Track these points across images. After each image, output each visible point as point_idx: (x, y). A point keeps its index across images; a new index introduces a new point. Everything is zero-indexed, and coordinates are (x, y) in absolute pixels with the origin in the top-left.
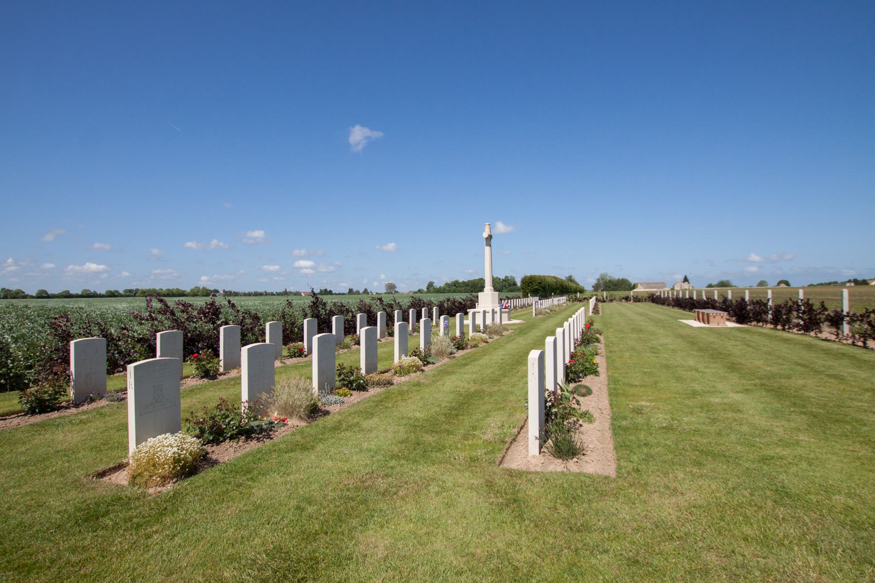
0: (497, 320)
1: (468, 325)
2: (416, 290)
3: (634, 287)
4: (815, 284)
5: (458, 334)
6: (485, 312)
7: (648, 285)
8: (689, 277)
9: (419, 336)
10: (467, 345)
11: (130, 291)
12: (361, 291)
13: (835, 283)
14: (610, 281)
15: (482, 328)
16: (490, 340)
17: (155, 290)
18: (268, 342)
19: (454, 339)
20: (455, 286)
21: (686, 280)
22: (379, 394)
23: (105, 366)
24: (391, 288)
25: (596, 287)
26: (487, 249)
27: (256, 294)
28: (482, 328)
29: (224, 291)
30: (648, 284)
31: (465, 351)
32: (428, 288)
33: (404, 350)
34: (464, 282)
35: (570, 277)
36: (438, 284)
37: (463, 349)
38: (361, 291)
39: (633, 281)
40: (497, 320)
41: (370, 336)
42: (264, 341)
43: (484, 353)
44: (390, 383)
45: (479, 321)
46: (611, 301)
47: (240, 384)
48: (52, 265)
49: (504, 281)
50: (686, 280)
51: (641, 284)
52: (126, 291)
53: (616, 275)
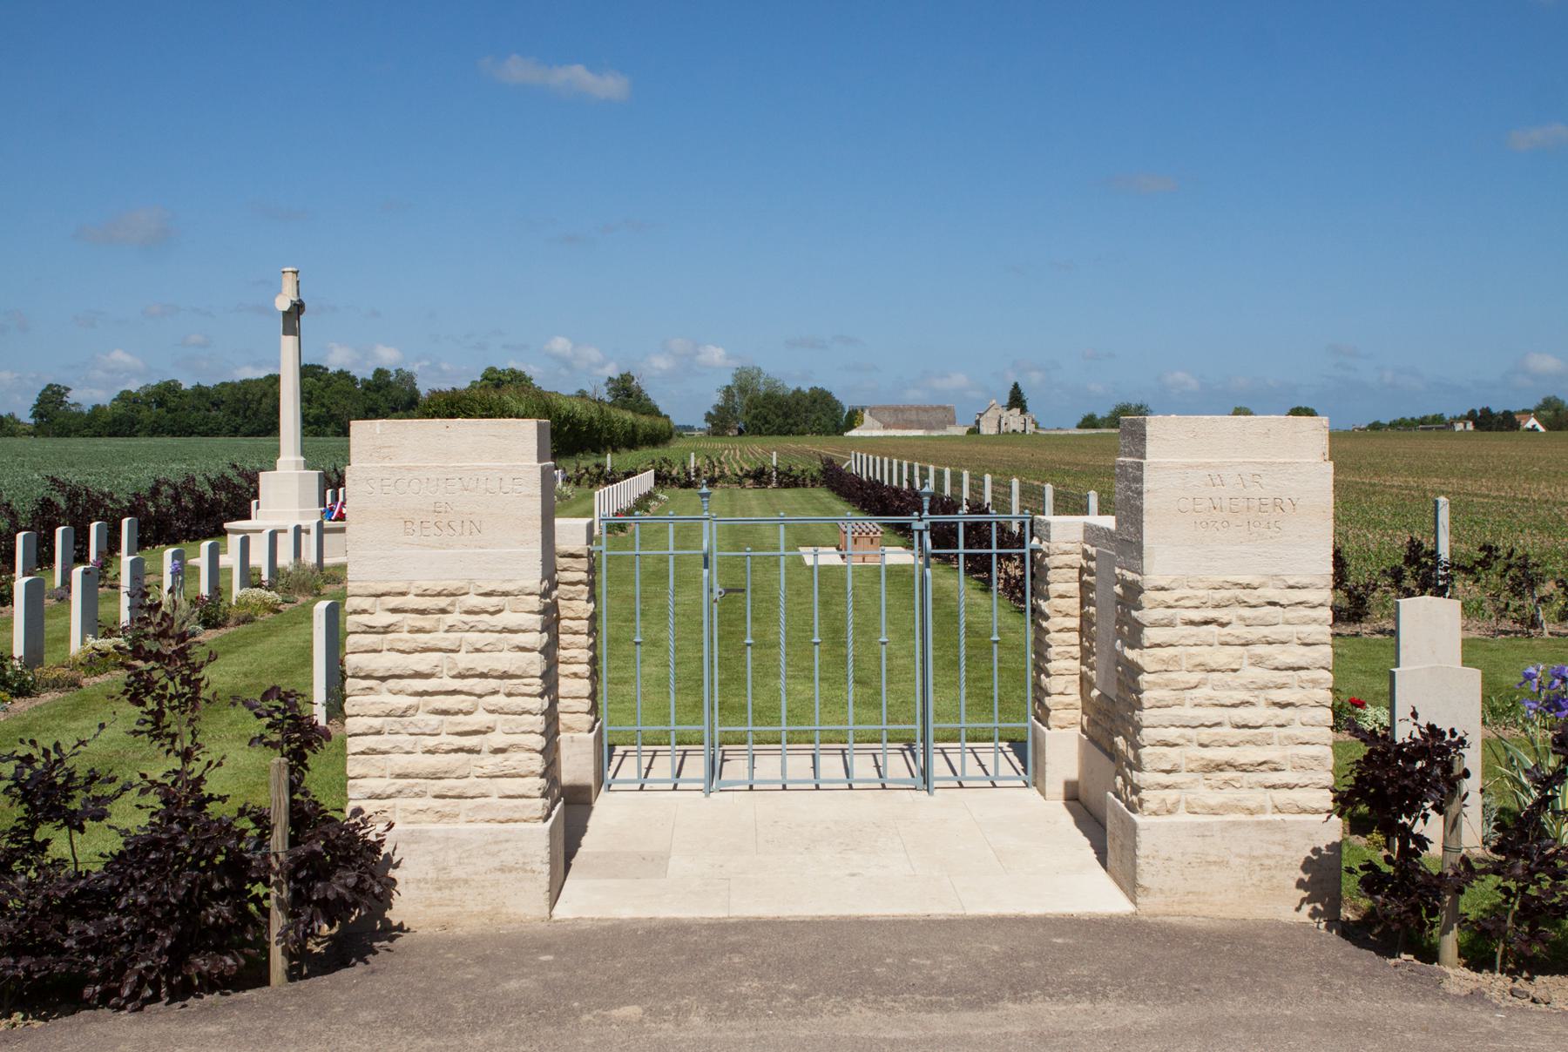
0: (309, 557)
1: (229, 570)
3: (853, 419)
4: (1386, 420)
5: (204, 590)
6: (273, 536)
7: (897, 415)
8: (1027, 395)
10: (227, 618)
13: (1438, 419)
14: (769, 397)
15: (265, 576)
16: (285, 607)
19: (196, 601)
20: (164, 412)
21: (1016, 400)
22: (55, 703)
25: (720, 422)
28: (265, 576)
30: (897, 410)
31: (223, 631)
33: (92, 624)
34: (200, 391)
35: (626, 379)
37: (217, 626)
39: (848, 402)
40: (309, 557)
41: (35, 593)
43: (269, 631)
44: (75, 684)
45: (259, 559)
46: (712, 482)
49: (368, 386)
50: (1016, 400)
51: (874, 411)
53: (792, 371)
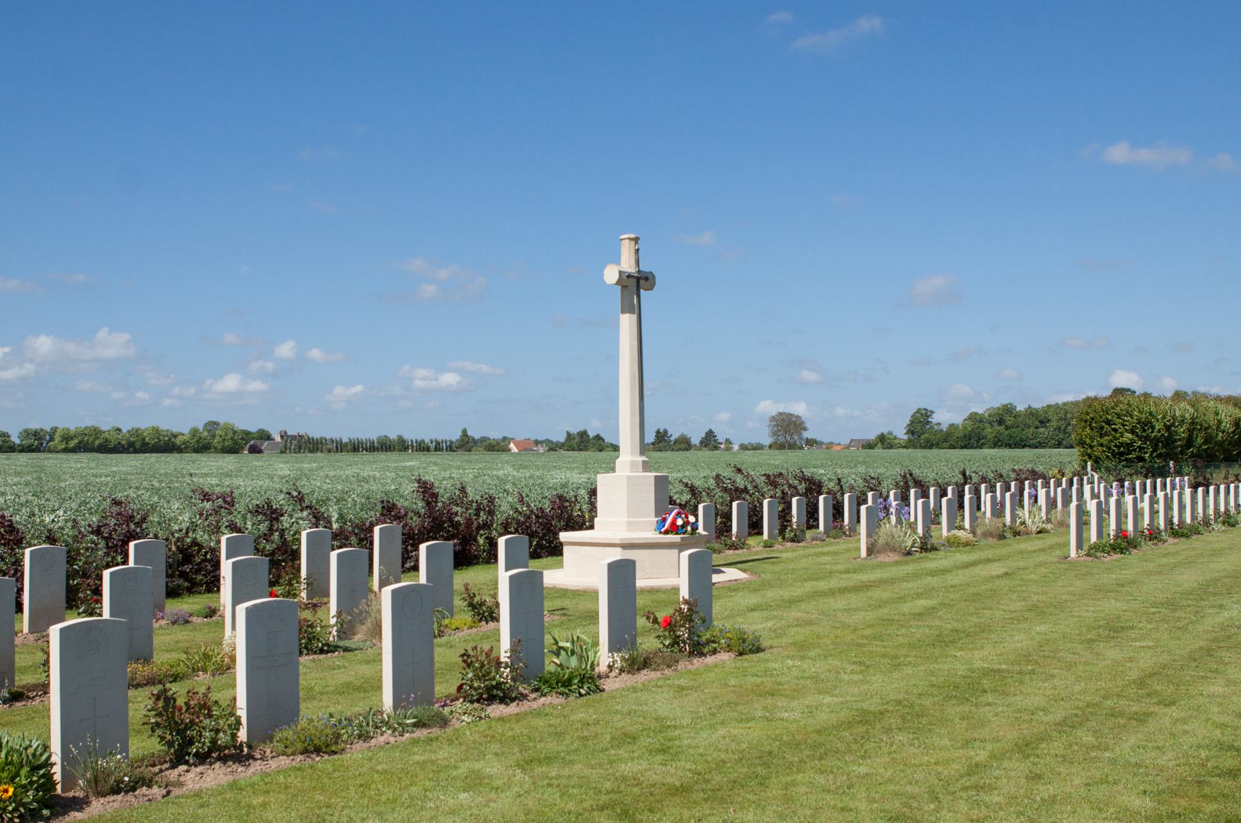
2: (872, 436)
9: (1068, 533)
11: (36, 434)
12: (696, 440)
17: (97, 432)
18: (106, 615)
23: (64, 605)
24: (788, 431)
26: (627, 322)
27: (385, 446)
29: (284, 435)
32: (911, 432)
34: (1031, 413)
36: (946, 417)
38: (696, 440)
42: (100, 615)
47: (380, 688)
48: (421, 377)
52: (27, 434)
